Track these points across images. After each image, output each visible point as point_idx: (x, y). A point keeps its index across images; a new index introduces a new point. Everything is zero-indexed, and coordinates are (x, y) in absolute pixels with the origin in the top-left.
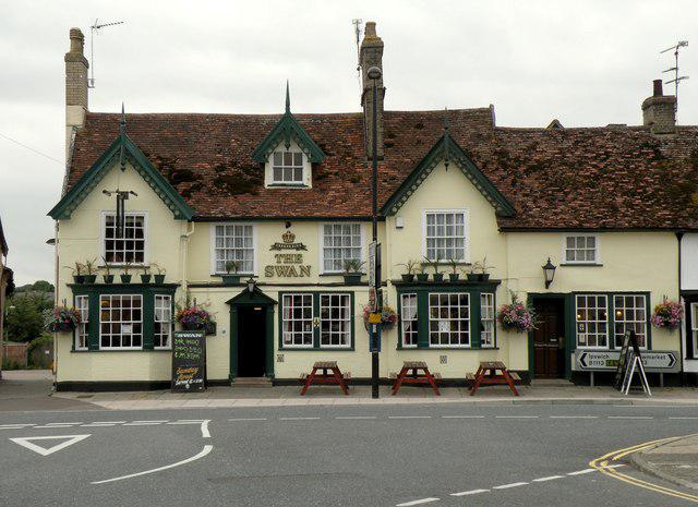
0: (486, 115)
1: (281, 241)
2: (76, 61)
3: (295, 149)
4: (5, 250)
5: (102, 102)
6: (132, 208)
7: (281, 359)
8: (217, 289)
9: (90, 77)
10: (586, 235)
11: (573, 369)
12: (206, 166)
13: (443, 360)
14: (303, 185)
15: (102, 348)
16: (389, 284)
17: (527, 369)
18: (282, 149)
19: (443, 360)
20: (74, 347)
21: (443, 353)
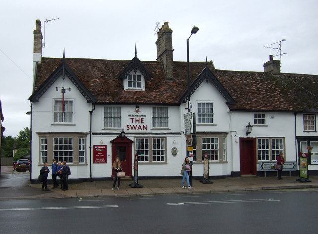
0: (11, 137)
2: (38, 34)
3: (138, 73)
4: (3, 119)
5: (47, 53)
6: (69, 95)
8: (173, 136)
10: (262, 113)
11: (258, 170)
12: (101, 82)
16: (182, 134)
17: (240, 170)
18: (132, 73)
20: (39, 163)
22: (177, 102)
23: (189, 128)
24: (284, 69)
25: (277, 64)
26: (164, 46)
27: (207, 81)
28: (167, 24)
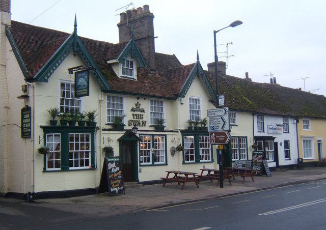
1: (135, 107)
7: (140, 172)
14: (133, 79)
15: (48, 169)
16: (179, 132)
20: (45, 169)
22: (173, 96)
24: (229, 72)
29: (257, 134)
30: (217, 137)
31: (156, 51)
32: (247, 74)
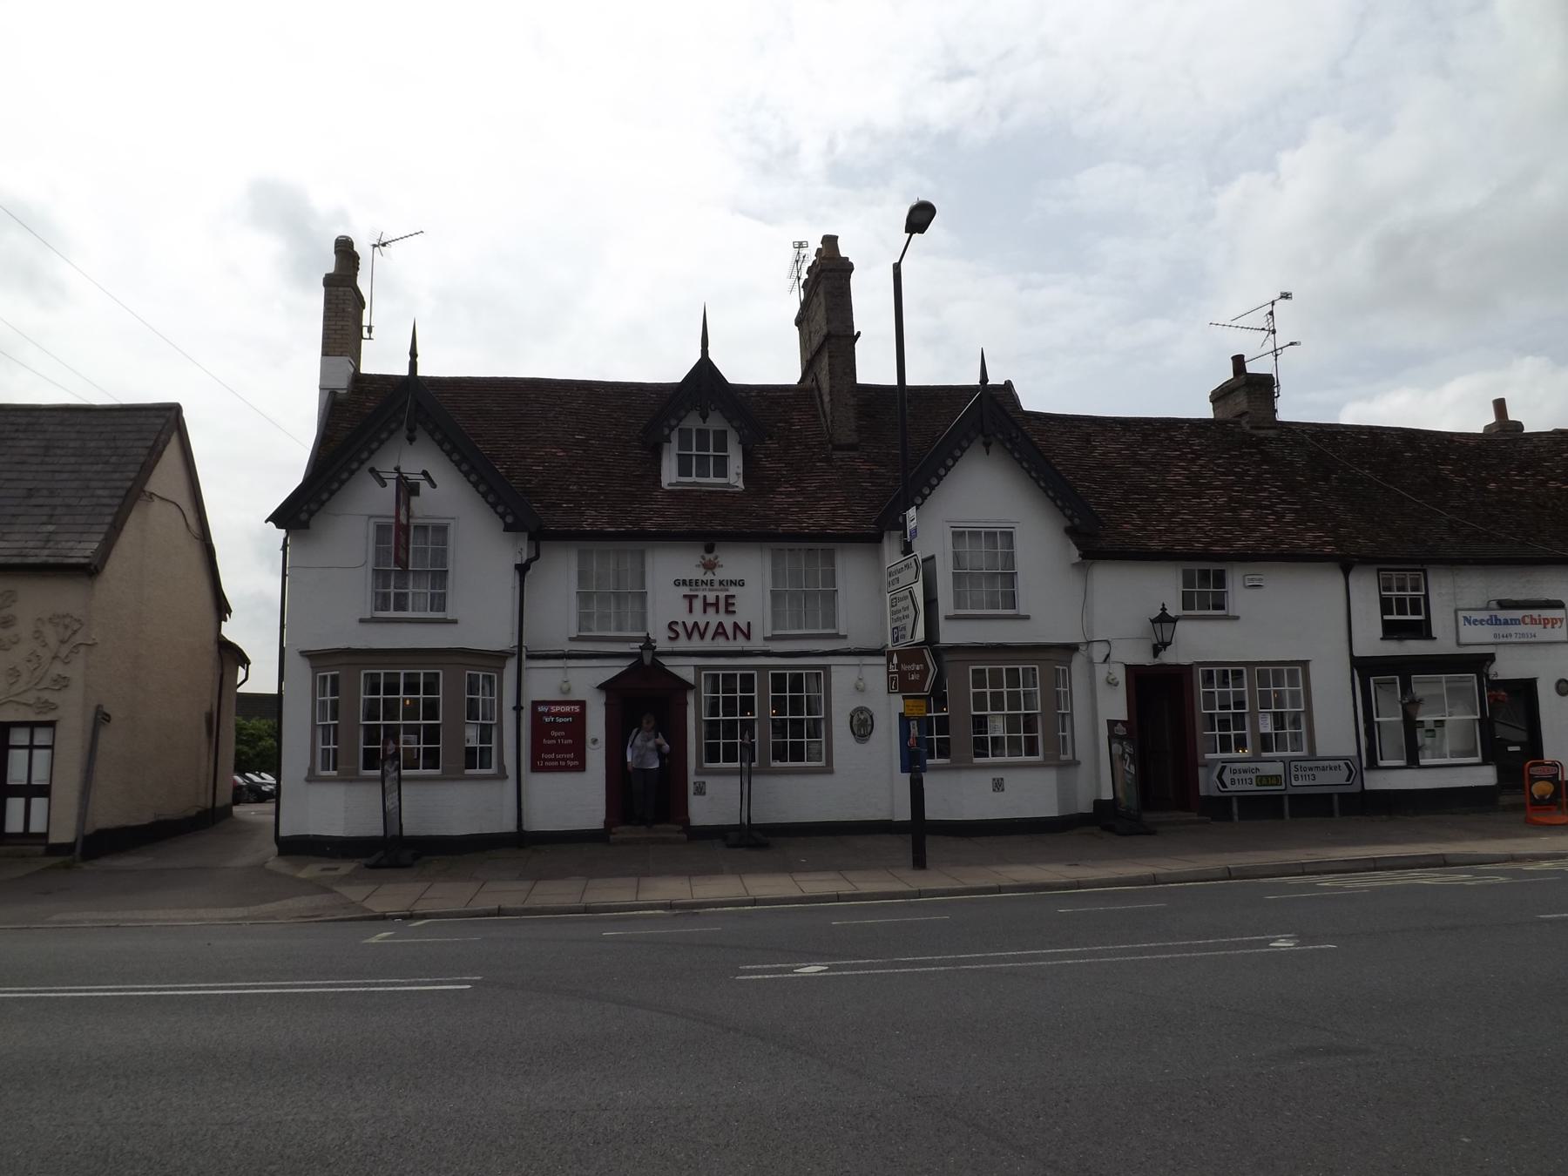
3: (715, 423)
5: (382, 357)
6: (428, 504)
7: (700, 790)
9: (365, 322)
10: (1213, 566)
11: (1203, 792)
12: (562, 457)
13: (998, 785)
19: (998, 785)
20: (312, 770)
21: (998, 774)
22: (869, 528)
23: (909, 622)
24: (1291, 408)
25: (1264, 387)
26: (823, 323)
27: (987, 445)
28: (830, 241)
29: (1370, 642)
30: (904, 667)
31: (861, 380)
32: (1500, 406)
